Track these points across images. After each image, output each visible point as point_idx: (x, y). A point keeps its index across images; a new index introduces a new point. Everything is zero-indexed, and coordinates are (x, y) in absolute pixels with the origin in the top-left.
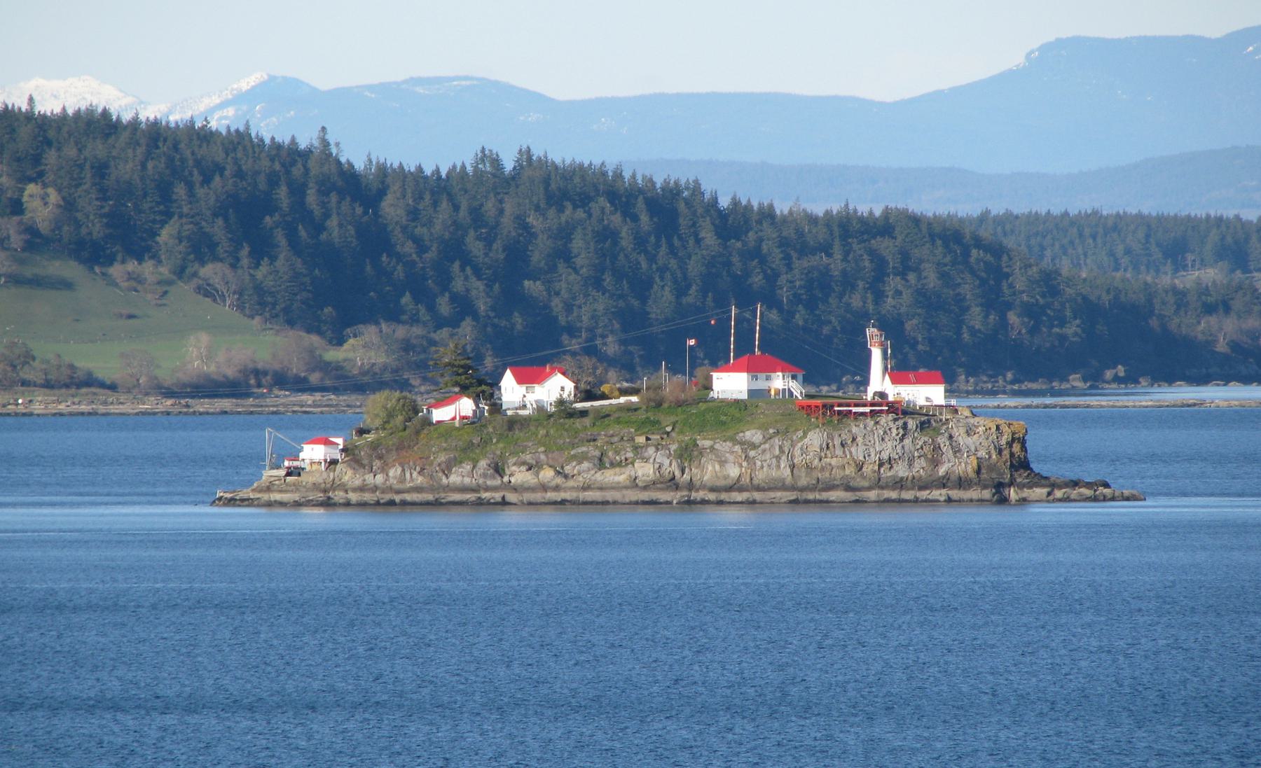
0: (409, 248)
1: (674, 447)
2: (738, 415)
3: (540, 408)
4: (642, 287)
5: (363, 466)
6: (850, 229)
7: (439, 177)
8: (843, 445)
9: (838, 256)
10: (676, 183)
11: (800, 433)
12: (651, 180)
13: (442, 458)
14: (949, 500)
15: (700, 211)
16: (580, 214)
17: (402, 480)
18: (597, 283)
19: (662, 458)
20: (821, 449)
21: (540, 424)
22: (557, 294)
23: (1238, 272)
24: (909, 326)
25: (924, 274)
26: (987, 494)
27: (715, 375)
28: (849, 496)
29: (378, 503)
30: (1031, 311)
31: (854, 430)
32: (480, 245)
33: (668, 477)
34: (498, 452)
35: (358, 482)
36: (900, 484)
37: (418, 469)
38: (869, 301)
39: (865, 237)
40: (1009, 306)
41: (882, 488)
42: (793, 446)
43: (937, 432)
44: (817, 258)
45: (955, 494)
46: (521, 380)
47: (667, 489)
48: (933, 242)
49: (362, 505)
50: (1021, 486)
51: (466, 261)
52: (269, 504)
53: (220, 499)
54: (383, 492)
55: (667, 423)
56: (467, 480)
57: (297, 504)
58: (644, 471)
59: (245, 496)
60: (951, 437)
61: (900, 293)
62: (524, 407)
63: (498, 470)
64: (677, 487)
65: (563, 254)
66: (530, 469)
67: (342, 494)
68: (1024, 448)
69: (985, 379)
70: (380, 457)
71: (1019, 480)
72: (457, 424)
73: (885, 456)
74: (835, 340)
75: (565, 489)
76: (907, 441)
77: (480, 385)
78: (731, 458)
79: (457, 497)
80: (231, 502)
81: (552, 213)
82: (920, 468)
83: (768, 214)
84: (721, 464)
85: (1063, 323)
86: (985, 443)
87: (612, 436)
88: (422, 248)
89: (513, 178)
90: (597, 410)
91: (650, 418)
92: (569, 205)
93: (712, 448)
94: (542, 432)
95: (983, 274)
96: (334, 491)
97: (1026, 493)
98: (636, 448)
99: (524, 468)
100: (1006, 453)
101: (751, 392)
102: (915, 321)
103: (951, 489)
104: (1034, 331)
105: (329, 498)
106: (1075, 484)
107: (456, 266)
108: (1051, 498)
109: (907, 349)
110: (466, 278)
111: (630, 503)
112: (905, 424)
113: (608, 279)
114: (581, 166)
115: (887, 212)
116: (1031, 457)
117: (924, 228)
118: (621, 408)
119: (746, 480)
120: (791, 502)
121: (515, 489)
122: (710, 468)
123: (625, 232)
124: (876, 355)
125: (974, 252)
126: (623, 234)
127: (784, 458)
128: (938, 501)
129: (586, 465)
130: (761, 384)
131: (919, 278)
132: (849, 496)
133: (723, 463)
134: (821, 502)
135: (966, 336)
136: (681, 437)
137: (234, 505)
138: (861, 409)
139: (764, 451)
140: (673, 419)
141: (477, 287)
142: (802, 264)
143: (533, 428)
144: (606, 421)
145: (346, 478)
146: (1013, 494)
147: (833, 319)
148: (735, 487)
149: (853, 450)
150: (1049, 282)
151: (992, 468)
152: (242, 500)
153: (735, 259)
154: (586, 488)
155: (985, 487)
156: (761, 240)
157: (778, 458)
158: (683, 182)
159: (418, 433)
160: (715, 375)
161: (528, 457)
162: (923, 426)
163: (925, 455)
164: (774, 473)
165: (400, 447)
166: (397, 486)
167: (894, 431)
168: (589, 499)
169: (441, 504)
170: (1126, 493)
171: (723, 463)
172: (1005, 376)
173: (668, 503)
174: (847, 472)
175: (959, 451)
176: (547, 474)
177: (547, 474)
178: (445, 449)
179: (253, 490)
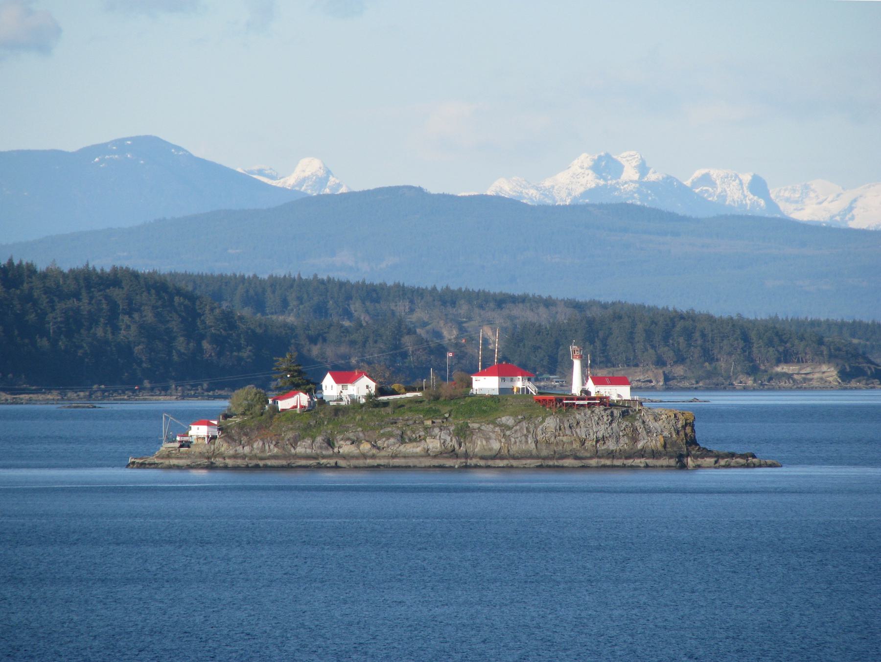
1: (452, 428)
2: (494, 406)
5: (234, 441)
6: (90, 282)
8: (570, 427)
9: (85, 300)
11: (540, 419)
13: (290, 435)
14: (647, 466)
17: (263, 450)
19: (444, 435)
20: (556, 430)
21: (356, 412)
23: (259, 315)
24: (137, 349)
25: (144, 314)
26: (673, 462)
27: (474, 378)
28: (577, 463)
29: (247, 467)
30: (217, 340)
31: (578, 416)
33: (450, 449)
34: (329, 431)
35: (232, 452)
36: (611, 455)
37: (274, 443)
38: (109, 332)
39: (102, 287)
40: (202, 337)
41: (599, 457)
44: (71, 301)
45: (651, 462)
46: (338, 380)
47: (451, 457)
49: (236, 468)
50: (696, 457)
52: (170, 467)
53: (133, 463)
54: (250, 459)
55: (445, 410)
56: (309, 451)
57: (189, 467)
58: (434, 444)
59: (152, 461)
60: (644, 422)
61: (129, 326)
62: (341, 399)
63: (330, 443)
64: (457, 456)
66: (353, 443)
68: (693, 431)
69: (188, 387)
70: (246, 434)
71: (693, 452)
72: (298, 412)
73: (600, 435)
74: (86, 360)
75: (380, 458)
76: (614, 425)
77: (308, 384)
78: (493, 436)
79: (303, 462)
80: (142, 466)
82: (624, 443)
83: (31, 270)
84: (487, 440)
85: (239, 348)
87: (407, 420)
90: (396, 401)
91: (432, 407)
94: (358, 417)
95: (183, 314)
96: (215, 457)
97: (700, 461)
98: (426, 429)
99: (349, 443)
100: (682, 433)
101: (501, 390)
102: (140, 347)
103: (648, 458)
104: (220, 354)
105: (212, 463)
106: (732, 455)
108: (717, 465)
109: (135, 366)
111: (425, 467)
112: (612, 412)
115: (115, 269)
116: (698, 436)
119: (504, 452)
120: (537, 467)
121: (344, 457)
122: (479, 443)
124: (577, 364)
125: (176, 299)
127: (530, 436)
128: (639, 467)
129: (392, 440)
130: (507, 385)
131: (141, 317)
132: (577, 463)
133: (488, 439)
134: (558, 467)
135: (175, 358)
136: (456, 421)
137: (144, 468)
138: (581, 402)
139: (516, 431)
140: (448, 408)
142: (60, 306)
143: (352, 415)
145: (223, 449)
146: (690, 461)
147: (85, 345)
148: (497, 456)
149: (578, 430)
150: (229, 320)
151: (674, 444)
152: (150, 464)
155: (671, 457)
156: (31, 288)
157: (526, 436)
159: (271, 417)
160: (474, 378)
161: (351, 435)
162: (624, 414)
163: (627, 435)
164: (524, 447)
166: (260, 455)
167: (605, 418)
168: (397, 464)
169: (292, 467)
170: (769, 461)
171: (488, 439)
172: (202, 385)
173: (451, 467)
174: (574, 446)
175: (650, 432)
176: (366, 447)
177: (366, 447)
178: (292, 429)
179: (157, 457)
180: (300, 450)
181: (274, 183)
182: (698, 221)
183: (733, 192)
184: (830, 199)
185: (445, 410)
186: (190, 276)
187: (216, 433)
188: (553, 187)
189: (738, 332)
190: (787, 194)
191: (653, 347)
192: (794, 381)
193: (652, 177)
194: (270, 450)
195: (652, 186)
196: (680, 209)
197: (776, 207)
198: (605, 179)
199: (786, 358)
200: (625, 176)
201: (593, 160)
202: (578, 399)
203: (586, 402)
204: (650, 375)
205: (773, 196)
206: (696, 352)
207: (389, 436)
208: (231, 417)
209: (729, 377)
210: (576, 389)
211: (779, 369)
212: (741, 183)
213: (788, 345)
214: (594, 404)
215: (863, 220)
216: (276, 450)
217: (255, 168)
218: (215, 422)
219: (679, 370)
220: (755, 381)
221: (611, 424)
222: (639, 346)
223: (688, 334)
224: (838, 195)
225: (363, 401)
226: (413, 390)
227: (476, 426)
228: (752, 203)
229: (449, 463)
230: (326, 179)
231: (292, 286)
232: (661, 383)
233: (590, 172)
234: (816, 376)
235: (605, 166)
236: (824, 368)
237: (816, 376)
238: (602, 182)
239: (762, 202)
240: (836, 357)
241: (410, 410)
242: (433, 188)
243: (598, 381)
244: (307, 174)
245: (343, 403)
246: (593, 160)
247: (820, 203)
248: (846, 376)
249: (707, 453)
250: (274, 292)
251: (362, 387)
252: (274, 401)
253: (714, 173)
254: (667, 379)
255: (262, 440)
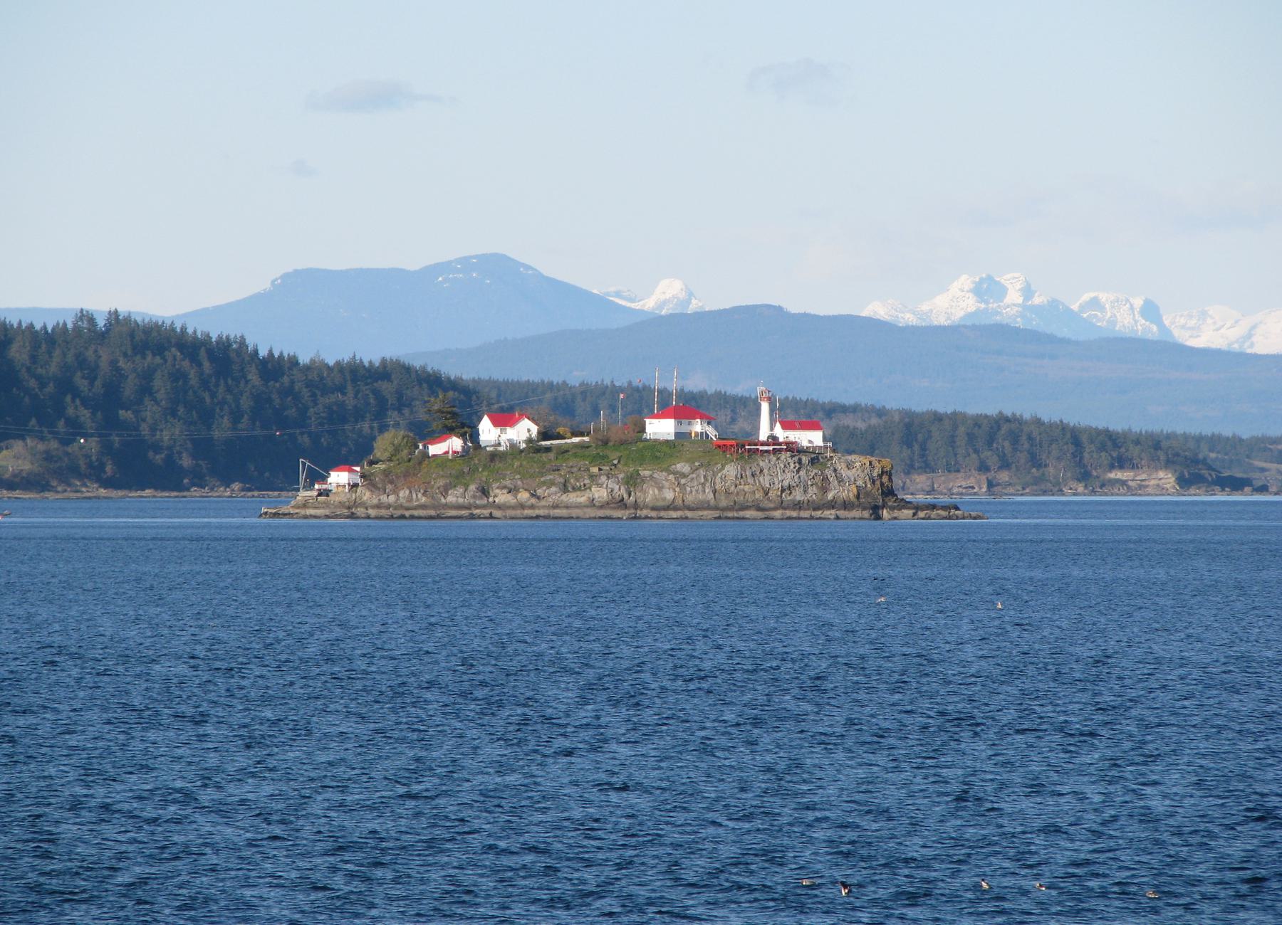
0: (33, 383)
1: (621, 476)
3: (513, 446)
4: (207, 417)
7: (46, 332)
10: (228, 337)
11: (719, 466)
12: (208, 335)
13: (441, 482)
14: (837, 518)
15: (247, 359)
16: (158, 360)
17: (410, 499)
18: (174, 413)
22: (144, 420)
26: (866, 514)
27: (648, 421)
28: (760, 514)
31: (762, 464)
32: (86, 382)
33: (618, 499)
35: (375, 501)
36: (798, 506)
41: (785, 509)
42: (714, 475)
43: (824, 465)
45: (841, 513)
46: (496, 422)
48: (420, 385)
50: (892, 508)
51: (76, 394)
52: (306, 517)
54: (395, 509)
55: (614, 456)
56: (461, 500)
58: (600, 494)
60: (835, 470)
62: (499, 444)
63: (485, 492)
64: (626, 507)
65: (146, 390)
67: (363, 510)
68: (890, 480)
70: (391, 482)
73: (786, 483)
75: (539, 508)
76: (802, 473)
78: (666, 484)
80: (276, 515)
81: (138, 358)
82: (813, 493)
83: (293, 362)
84: (659, 489)
86: (862, 475)
88: (42, 386)
89: (108, 330)
90: (559, 446)
92: (149, 353)
93: (651, 477)
94: (516, 464)
97: (896, 513)
98: (592, 477)
100: (878, 483)
101: (677, 434)
107: (68, 398)
110: (76, 408)
112: (800, 460)
113: (181, 411)
114: (156, 324)
115: (384, 361)
117: (413, 376)
118: (576, 445)
121: (499, 507)
123: (192, 373)
126: (192, 376)
129: (553, 489)
130: (684, 429)
131: (412, 412)
133: (661, 488)
136: (625, 469)
140: (618, 454)
141: (85, 414)
142: (324, 401)
144: (566, 455)
148: (671, 507)
151: (868, 494)
153: (274, 396)
154: (555, 506)
155: (864, 509)
156: (292, 382)
157: (703, 485)
158: (232, 337)
159: (420, 463)
160: (648, 421)
161: (508, 483)
162: (814, 461)
164: (701, 497)
165: (406, 475)
171: (661, 488)
176: (524, 496)
177: (524, 496)
180: (451, 499)
181: (633, 305)
182: (1077, 343)
183: (1125, 318)
184: (1228, 325)
185: (614, 456)
186: (494, 382)
187: (359, 481)
188: (931, 311)
189: (1068, 435)
190: (1182, 321)
191: (976, 451)
192: (1129, 487)
193: (1037, 300)
194: (418, 500)
195: (1037, 309)
196: (1064, 332)
197: (1169, 332)
198: (987, 302)
199: (1121, 463)
200: (1008, 300)
201: (974, 282)
202: (763, 444)
203: (771, 448)
204: (971, 482)
205: (1167, 322)
206: (1023, 457)
207: (551, 484)
208: (376, 463)
209: (1059, 484)
210: (764, 435)
211: (1112, 475)
212: (1132, 307)
213: (1123, 450)
214: (780, 450)
215: (1264, 345)
216: (424, 499)
217: (612, 289)
218: (358, 469)
219: (1004, 476)
220: (1086, 487)
221: (798, 471)
222: (961, 451)
223: (1015, 439)
224: (1236, 322)
225: (523, 446)
226: (582, 434)
227: (647, 473)
228: (1143, 328)
229: (618, 514)
230: (689, 302)
231: (604, 393)
232: (984, 490)
233: (971, 295)
234: (1153, 482)
235: (987, 289)
236: (1161, 474)
237: (1153, 482)
238: (983, 306)
239: (1155, 328)
240: (1173, 463)
241: (575, 455)
242: (794, 307)
243: (787, 426)
244: (668, 296)
245: (501, 449)
246: (974, 282)
247: (1218, 330)
248: (1184, 483)
249: (905, 504)
250: (584, 400)
251: (523, 431)
252: (425, 447)
253: (1103, 297)
254: (991, 485)
255: (409, 488)
